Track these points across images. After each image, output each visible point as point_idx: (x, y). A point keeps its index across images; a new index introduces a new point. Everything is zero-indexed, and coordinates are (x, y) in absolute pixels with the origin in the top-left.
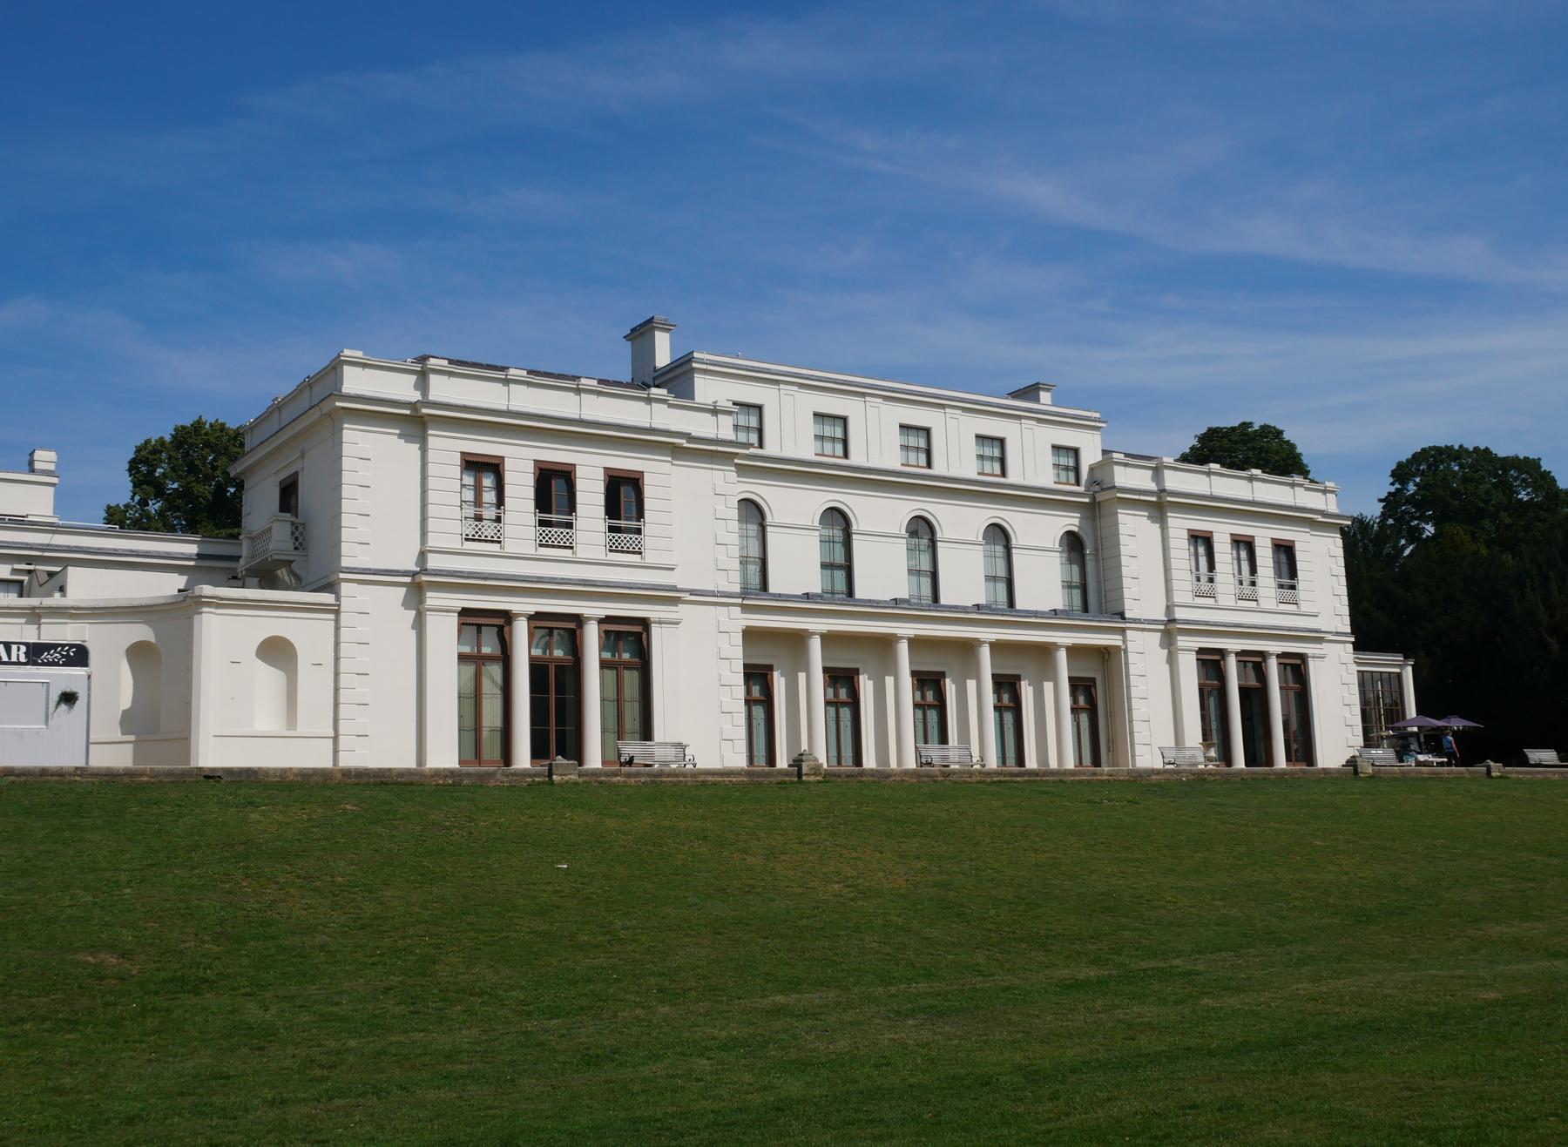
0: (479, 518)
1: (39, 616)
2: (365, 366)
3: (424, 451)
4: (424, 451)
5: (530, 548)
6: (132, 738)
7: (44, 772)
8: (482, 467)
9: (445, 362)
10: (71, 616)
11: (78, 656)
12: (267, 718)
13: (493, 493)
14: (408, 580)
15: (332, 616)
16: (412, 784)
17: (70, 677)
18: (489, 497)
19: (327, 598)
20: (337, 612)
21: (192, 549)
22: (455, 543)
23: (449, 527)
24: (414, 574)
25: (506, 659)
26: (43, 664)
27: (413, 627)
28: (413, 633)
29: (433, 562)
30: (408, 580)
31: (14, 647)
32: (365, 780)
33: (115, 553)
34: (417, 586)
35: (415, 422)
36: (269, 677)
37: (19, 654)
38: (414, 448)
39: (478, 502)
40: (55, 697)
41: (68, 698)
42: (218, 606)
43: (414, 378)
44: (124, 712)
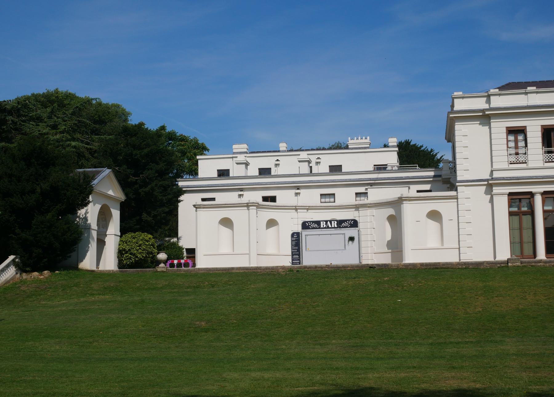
0: (517, 154)
1: (358, 208)
2: (463, 98)
3: (490, 128)
4: (490, 128)
5: (541, 164)
6: (390, 251)
7: (316, 267)
8: (516, 132)
9: (497, 90)
10: (369, 207)
11: (354, 224)
12: (434, 242)
13: (524, 142)
14: (486, 183)
15: (456, 200)
16: (448, 268)
17: (351, 232)
18: (521, 144)
19: (453, 193)
20: (457, 199)
21: (432, 174)
22: (506, 166)
23: (502, 159)
24: (487, 180)
25: (532, 213)
26: (343, 227)
27: (490, 202)
28: (490, 205)
29: (496, 175)
30: (486, 183)
31: (333, 222)
32: (429, 267)
33: (401, 178)
34: (490, 185)
35: (485, 118)
36: (433, 225)
37: (335, 224)
38: (486, 128)
39: (516, 147)
40: (347, 239)
41: (352, 239)
42: (410, 200)
43: (485, 99)
44: (388, 241)
